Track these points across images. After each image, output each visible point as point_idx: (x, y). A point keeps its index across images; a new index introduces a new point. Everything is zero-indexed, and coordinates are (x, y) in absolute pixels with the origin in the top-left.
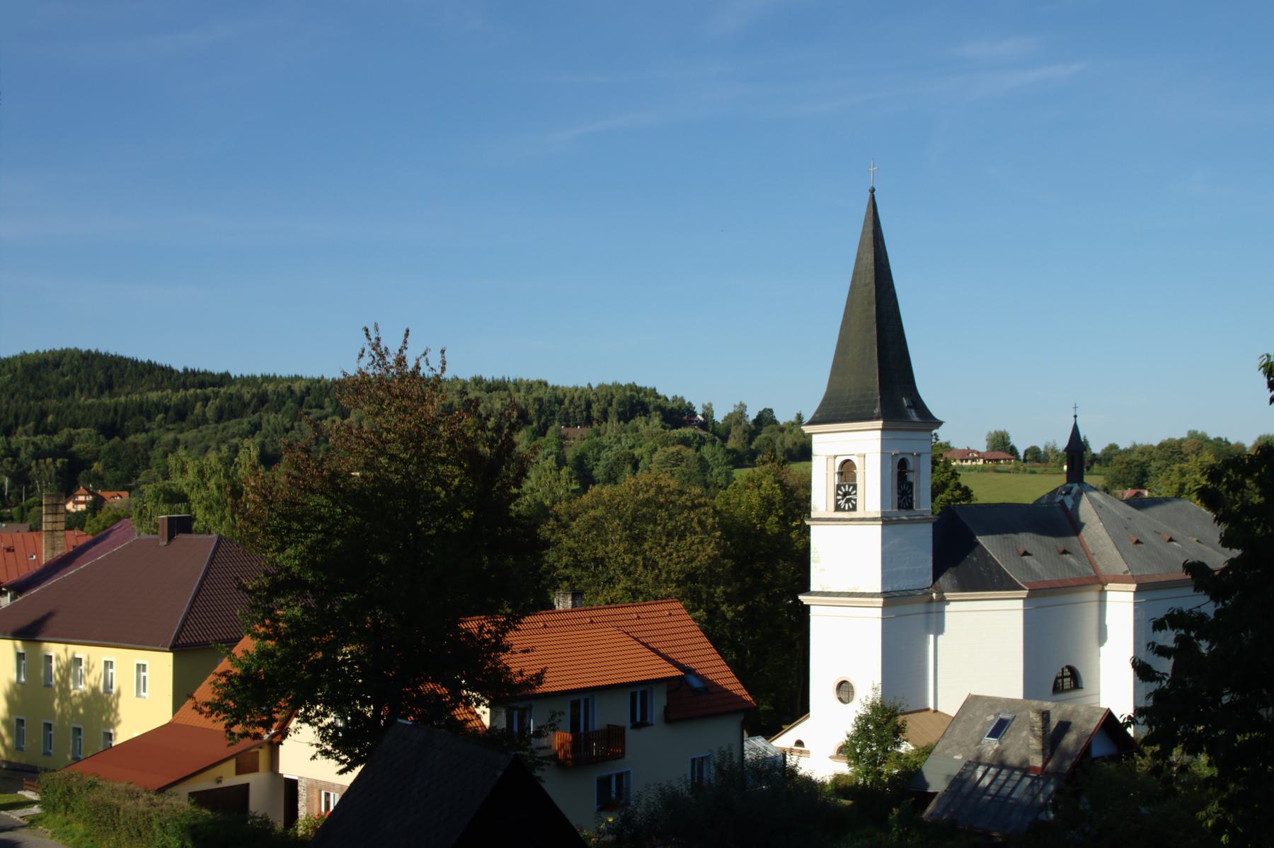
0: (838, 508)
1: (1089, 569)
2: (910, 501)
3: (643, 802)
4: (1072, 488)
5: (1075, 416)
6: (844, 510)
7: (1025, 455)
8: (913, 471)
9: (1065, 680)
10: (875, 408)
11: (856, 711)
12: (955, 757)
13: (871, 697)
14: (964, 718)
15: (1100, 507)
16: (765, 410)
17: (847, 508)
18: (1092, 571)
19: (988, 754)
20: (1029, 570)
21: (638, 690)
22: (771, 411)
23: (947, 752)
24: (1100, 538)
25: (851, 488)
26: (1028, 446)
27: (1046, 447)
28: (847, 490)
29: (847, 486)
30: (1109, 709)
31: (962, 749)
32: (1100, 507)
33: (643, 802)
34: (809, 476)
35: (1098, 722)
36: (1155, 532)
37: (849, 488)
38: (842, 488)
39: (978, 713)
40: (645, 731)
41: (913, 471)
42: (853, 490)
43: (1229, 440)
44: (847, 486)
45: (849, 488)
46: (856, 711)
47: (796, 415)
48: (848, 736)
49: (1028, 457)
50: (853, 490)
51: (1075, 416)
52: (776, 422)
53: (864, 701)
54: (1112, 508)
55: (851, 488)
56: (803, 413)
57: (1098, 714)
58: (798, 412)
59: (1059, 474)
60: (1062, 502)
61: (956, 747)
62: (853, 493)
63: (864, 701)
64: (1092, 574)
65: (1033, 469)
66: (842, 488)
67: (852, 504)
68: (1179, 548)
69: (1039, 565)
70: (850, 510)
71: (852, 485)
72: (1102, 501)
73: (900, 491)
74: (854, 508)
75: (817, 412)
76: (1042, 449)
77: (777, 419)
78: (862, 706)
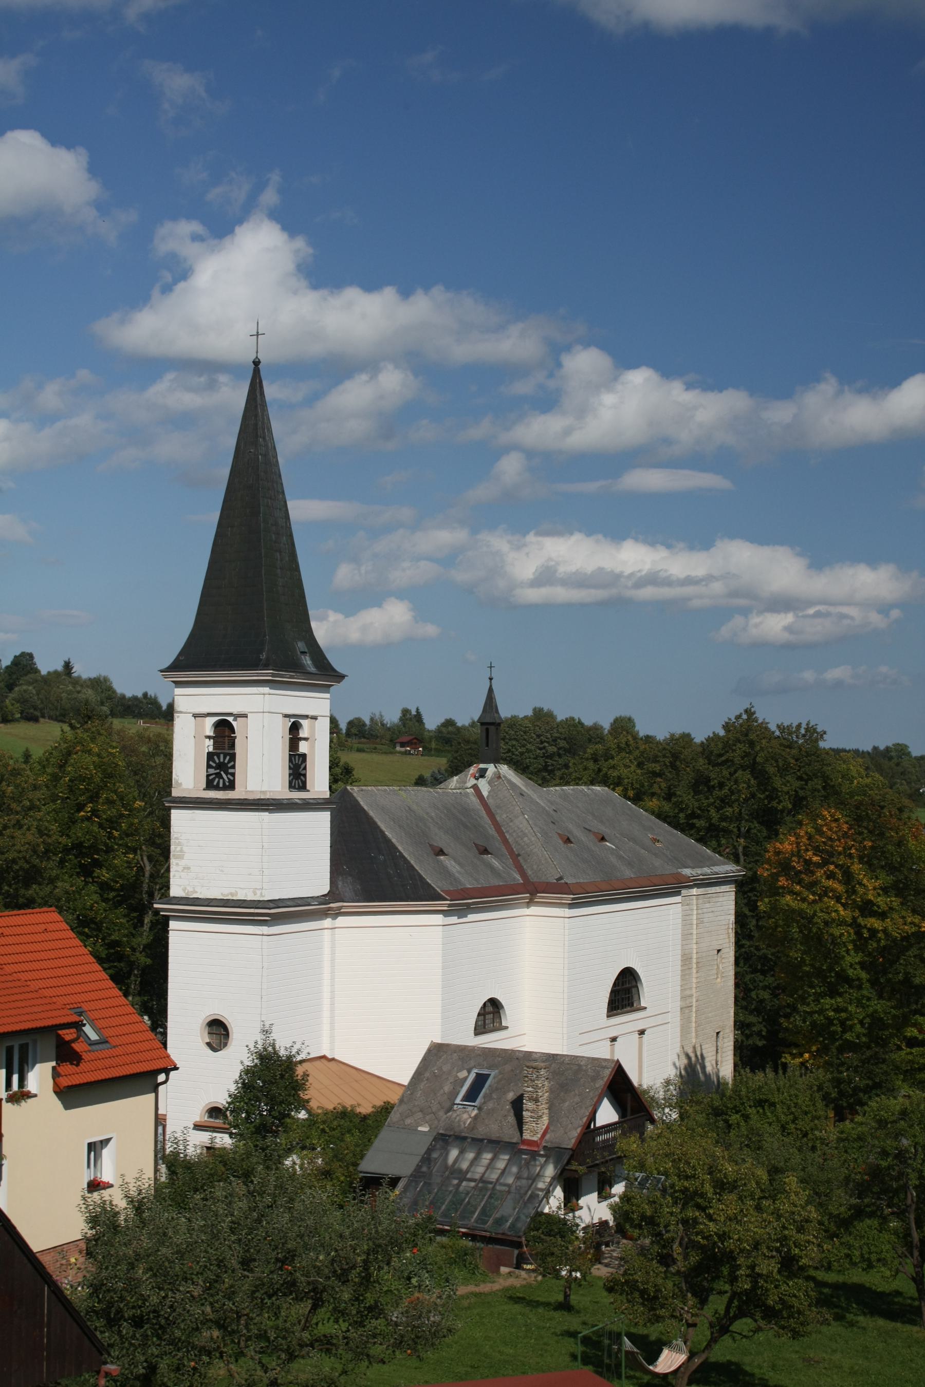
0: (210, 785)
1: (515, 875)
2: (303, 779)
3: (717, 1304)
4: (486, 770)
5: (491, 679)
6: (217, 788)
7: (348, 729)
8: (306, 739)
9: (487, 1017)
10: (261, 652)
11: (242, 1062)
12: (420, 1129)
13: (260, 1043)
14: (427, 1075)
15: (522, 795)
16: (23, 654)
17: (221, 785)
18: (518, 877)
19: (465, 1123)
20: (445, 873)
21: (16, 1044)
22: (31, 656)
23: (408, 1121)
24: (525, 835)
25: (228, 758)
26: (351, 718)
27: (372, 719)
28: (222, 760)
29: (222, 756)
30: (618, 1061)
31: (428, 1118)
32: (522, 795)
33: (717, 1304)
34: (169, 743)
35: (605, 1079)
36: (585, 828)
37: (225, 758)
38: (216, 758)
39: (446, 1068)
40: (27, 1105)
41: (306, 739)
42: (229, 762)
43: (583, 721)
44: (222, 756)
45: (225, 758)
46: (242, 1062)
47: (63, 663)
48: (230, 1096)
49: (354, 731)
50: (229, 762)
51: (491, 679)
52: (37, 671)
53: (252, 1049)
54: (535, 797)
55: (228, 758)
56: (72, 661)
57: (605, 1067)
58: (67, 659)
59: (391, 753)
60: (475, 787)
61: (420, 1115)
62: (229, 765)
63: (252, 1049)
64: (518, 880)
65: (360, 746)
66: (216, 758)
67: (302, 780)
68: (612, 848)
69: (458, 867)
70: (225, 788)
71: (229, 754)
72: (523, 788)
73: (292, 766)
74: (231, 786)
75: (181, 654)
76: (368, 722)
77: (39, 668)
78: (249, 1055)
